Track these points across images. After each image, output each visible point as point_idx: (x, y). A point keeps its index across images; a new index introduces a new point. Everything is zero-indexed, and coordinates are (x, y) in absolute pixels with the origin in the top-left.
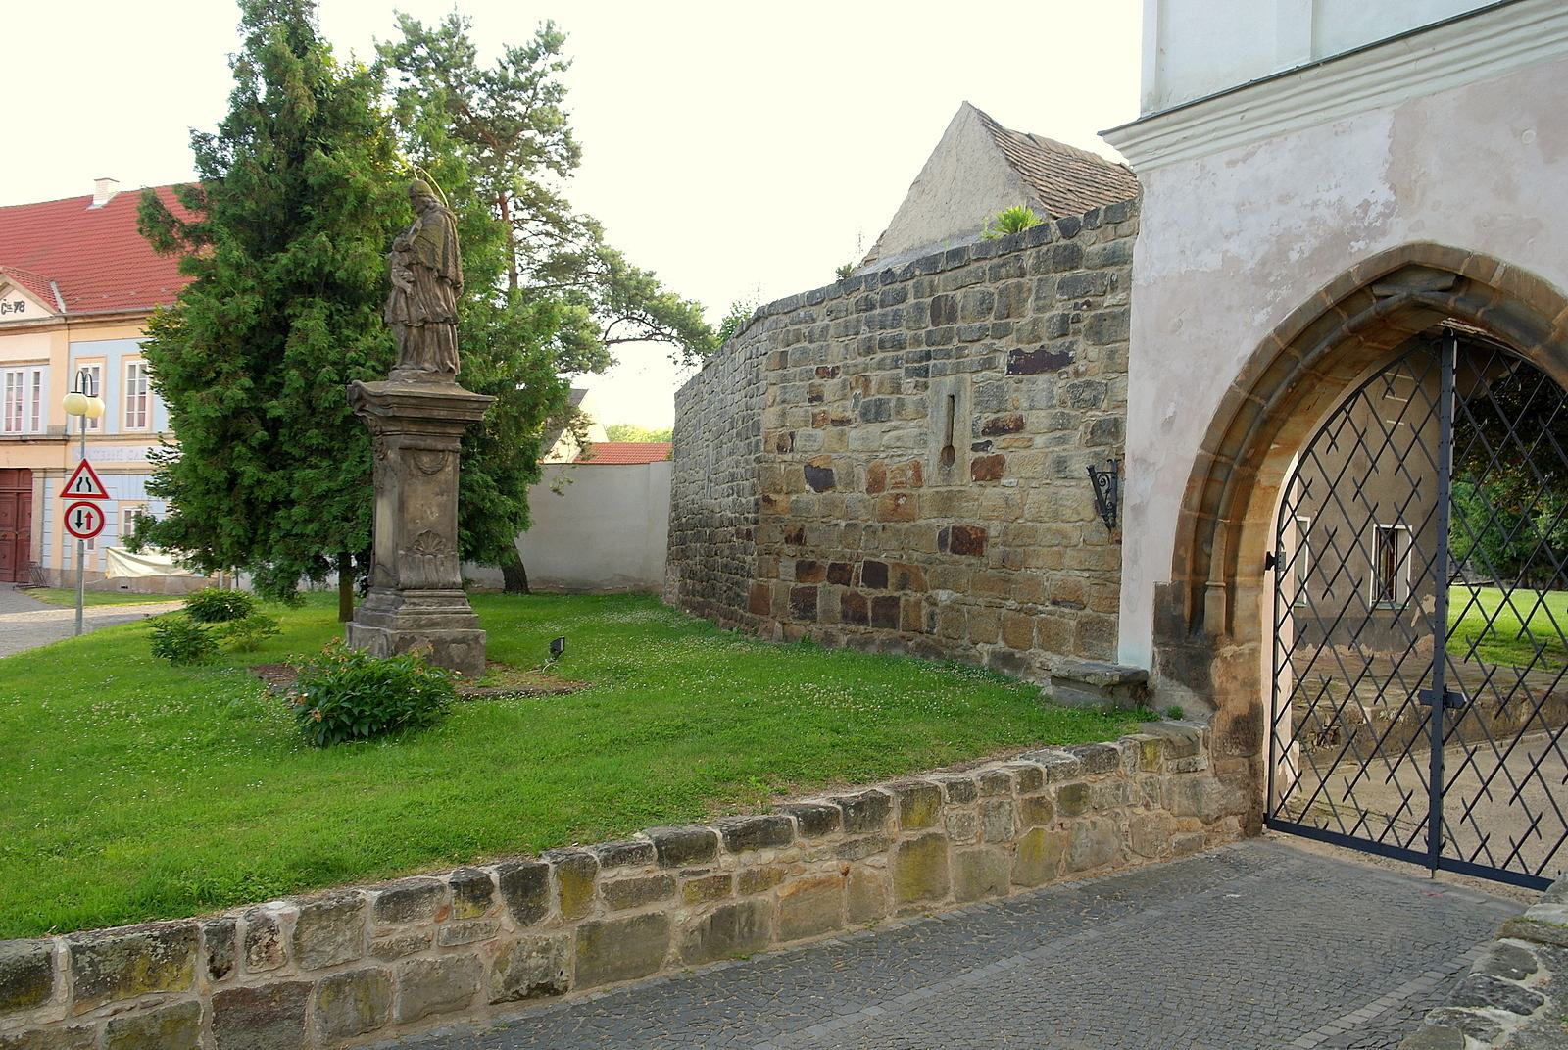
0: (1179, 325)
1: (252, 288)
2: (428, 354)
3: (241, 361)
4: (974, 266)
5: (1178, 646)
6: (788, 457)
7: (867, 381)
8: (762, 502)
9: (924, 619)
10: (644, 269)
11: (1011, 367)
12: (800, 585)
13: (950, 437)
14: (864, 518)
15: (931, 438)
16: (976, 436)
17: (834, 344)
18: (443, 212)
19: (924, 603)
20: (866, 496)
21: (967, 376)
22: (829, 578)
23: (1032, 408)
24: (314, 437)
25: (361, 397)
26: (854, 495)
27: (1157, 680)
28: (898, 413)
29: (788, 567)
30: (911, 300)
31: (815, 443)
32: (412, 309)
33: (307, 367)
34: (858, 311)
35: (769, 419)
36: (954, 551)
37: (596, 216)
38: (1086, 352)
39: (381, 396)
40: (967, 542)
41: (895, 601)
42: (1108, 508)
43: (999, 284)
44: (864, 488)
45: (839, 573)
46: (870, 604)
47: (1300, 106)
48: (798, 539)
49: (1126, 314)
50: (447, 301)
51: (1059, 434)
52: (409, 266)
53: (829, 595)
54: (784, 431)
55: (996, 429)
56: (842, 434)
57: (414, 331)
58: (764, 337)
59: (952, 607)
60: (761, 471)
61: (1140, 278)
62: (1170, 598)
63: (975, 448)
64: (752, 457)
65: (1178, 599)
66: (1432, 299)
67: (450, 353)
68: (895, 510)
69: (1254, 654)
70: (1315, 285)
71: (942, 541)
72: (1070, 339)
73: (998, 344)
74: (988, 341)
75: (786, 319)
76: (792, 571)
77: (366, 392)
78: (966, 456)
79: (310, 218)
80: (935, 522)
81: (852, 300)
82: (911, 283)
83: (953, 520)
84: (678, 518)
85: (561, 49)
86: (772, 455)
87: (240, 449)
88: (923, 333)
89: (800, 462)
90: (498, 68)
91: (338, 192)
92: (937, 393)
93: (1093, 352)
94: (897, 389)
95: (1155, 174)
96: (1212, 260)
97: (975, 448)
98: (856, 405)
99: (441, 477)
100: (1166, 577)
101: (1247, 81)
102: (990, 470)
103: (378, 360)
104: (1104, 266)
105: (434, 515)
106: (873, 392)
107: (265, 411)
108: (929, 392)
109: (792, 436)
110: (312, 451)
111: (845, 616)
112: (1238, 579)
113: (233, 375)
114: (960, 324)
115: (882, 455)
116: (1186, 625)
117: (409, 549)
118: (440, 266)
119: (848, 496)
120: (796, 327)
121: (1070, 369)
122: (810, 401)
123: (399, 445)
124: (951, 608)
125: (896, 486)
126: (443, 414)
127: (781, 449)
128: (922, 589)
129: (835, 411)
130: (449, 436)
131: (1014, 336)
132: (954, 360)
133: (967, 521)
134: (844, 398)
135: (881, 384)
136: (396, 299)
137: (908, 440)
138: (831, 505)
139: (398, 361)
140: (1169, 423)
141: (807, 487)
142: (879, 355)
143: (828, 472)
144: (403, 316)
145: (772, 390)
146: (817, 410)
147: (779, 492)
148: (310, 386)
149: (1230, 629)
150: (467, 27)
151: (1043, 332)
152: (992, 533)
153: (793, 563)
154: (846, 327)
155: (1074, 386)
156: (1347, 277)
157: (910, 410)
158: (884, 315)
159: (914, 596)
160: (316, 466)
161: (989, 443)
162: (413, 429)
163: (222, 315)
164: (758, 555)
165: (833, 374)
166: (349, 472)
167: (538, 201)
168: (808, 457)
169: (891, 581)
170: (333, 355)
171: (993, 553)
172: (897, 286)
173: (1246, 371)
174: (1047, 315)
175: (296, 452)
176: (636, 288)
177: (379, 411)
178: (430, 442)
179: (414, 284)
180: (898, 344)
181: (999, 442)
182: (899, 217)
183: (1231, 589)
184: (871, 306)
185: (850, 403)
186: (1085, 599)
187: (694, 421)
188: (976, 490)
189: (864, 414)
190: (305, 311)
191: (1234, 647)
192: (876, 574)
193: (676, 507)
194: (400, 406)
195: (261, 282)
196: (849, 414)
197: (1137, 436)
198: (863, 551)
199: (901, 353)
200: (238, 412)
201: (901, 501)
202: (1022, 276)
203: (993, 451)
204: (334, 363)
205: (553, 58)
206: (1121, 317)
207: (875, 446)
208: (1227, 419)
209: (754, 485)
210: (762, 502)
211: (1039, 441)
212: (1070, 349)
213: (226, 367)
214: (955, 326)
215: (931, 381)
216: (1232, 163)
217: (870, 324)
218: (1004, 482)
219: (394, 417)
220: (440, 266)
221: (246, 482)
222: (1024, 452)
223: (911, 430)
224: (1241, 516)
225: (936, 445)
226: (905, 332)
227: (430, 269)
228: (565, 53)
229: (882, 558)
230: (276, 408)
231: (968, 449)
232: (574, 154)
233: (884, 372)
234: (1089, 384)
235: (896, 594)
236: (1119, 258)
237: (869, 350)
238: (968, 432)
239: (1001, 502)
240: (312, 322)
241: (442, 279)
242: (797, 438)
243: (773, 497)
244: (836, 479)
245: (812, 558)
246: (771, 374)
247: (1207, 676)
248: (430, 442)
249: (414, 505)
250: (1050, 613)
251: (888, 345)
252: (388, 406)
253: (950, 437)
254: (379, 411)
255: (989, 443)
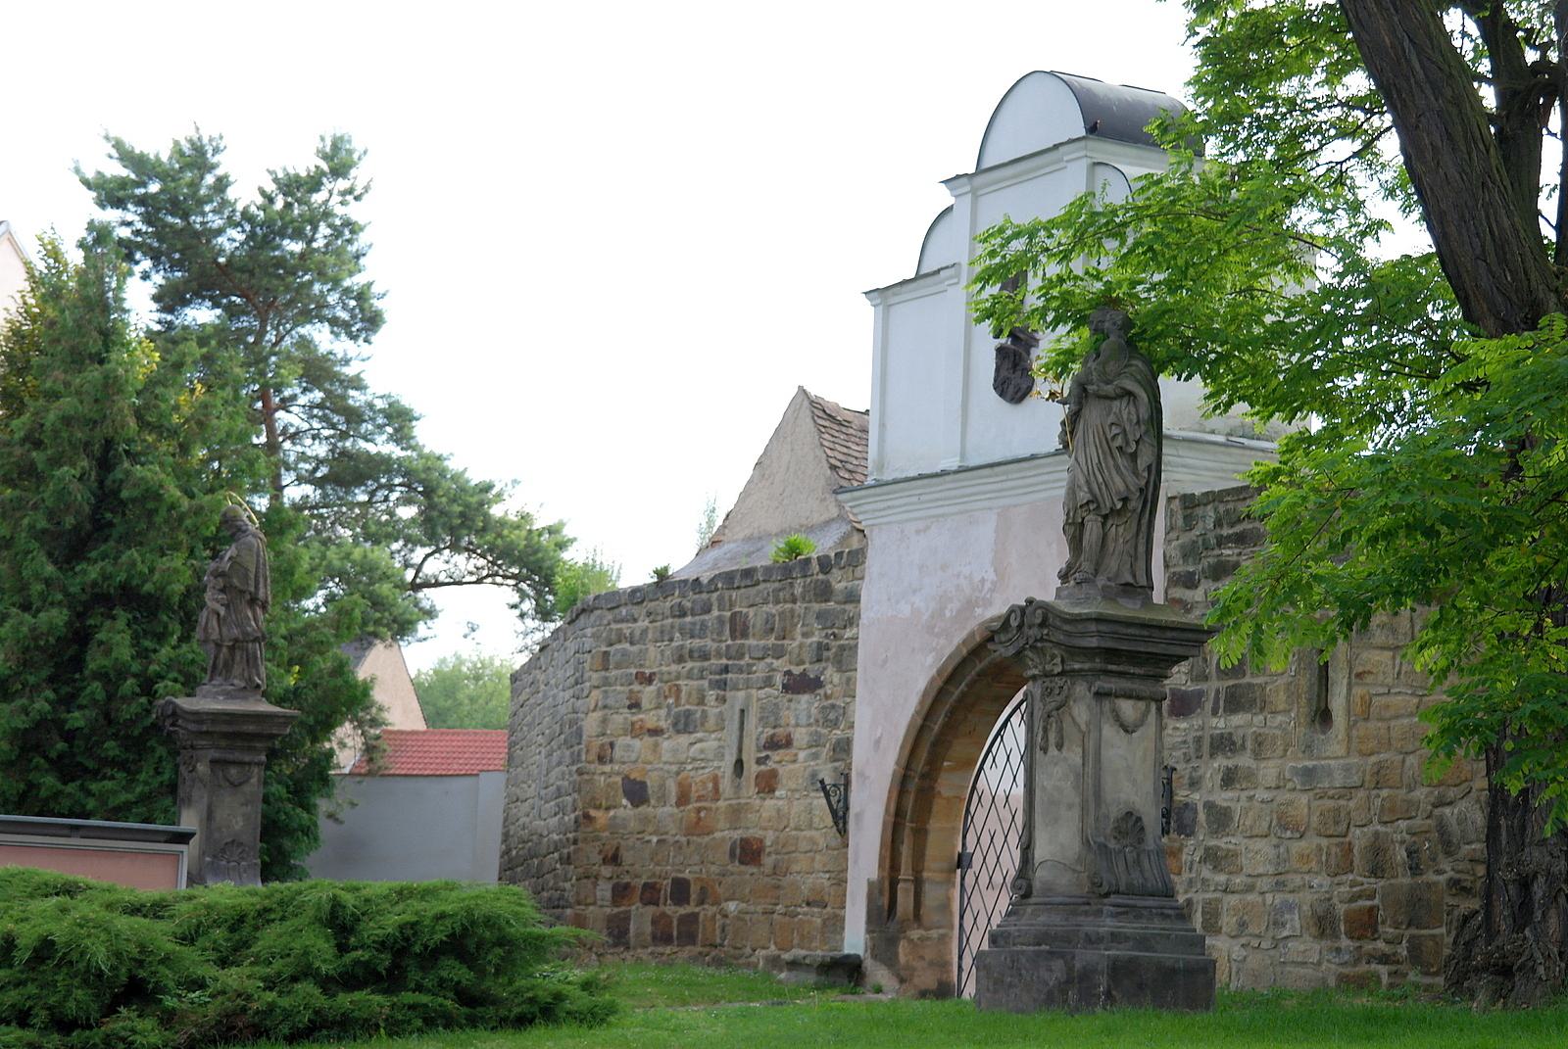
0: (885, 661)
1: (60, 603)
2: (237, 670)
3: (45, 673)
4: (762, 586)
6: (607, 768)
7: (679, 690)
8: (581, 820)
9: (718, 932)
10: (475, 478)
11: (785, 686)
12: (616, 910)
13: (740, 750)
14: (674, 834)
15: (727, 752)
16: (759, 751)
17: (652, 648)
18: (255, 536)
19: (718, 917)
20: (676, 810)
21: (754, 691)
22: (641, 899)
23: (797, 725)
24: (111, 748)
25: (176, 714)
26: (665, 809)
27: (869, 964)
28: (702, 724)
29: (604, 890)
30: (715, 613)
31: (632, 750)
32: (224, 630)
33: (111, 679)
34: (674, 617)
35: (591, 724)
36: (742, 862)
37: (406, 402)
38: (831, 675)
39: (196, 713)
40: (749, 852)
41: (695, 916)
42: (840, 818)
43: (778, 607)
44: (673, 800)
45: (650, 894)
46: (675, 923)
47: (955, 497)
48: (614, 859)
49: (856, 646)
50: (255, 620)
51: (814, 750)
52: (223, 591)
53: (641, 919)
54: (606, 740)
55: (773, 744)
56: (656, 745)
57: (225, 650)
58: (589, 631)
59: (740, 917)
60: (582, 782)
61: (864, 621)
63: (759, 761)
64: (574, 768)
65: (881, 892)
67: (257, 670)
68: (697, 823)
69: (944, 939)
70: (959, 637)
71: (732, 854)
72: (824, 664)
73: (776, 663)
74: (769, 660)
75: (610, 616)
76: (608, 894)
77: (182, 709)
78: (752, 769)
79: (111, 524)
80: (726, 834)
81: (668, 604)
82: (715, 595)
83: (739, 832)
84: (507, 852)
85: (353, 172)
86: (592, 766)
87: (38, 760)
88: (723, 645)
89: (618, 774)
90: (260, 200)
91: (150, 505)
92: (732, 707)
93: (836, 678)
94: (701, 701)
95: (876, 530)
96: (905, 610)
97: (759, 761)
98: (668, 714)
99: (246, 788)
100: (874, 875)
102: (768, 784)
103: (180, 672)
104: (845, 603)
105: (238, 824)
106: (683, 701)
107: (65, 721)
108: (726, 706)
109: (612, 745)
110: (113, 763)
111: (654, 938)
112: (925, 874)
113: (36, 689)
114: (751, 642)
115: (689, 767)
116: (885, 914)
117: (215, 856)
118: (252, 589)
119: (660, 810)
120: (619, 626)
121: (821, 691)
122: (630, 707)
123: (209, 757)
124: (738, 918)
125: (700, 799)
126: (251, 728)
127: (601, 759)
128: (716, 903)
129: (651, 719)
130: (255, 749)
131: (786, 658)
132: (744, 676)
133: (753, 833)
134: (658, 707)
135: (690, 694)
136: (207, 619)
137: (705, 753)
138: (645, 820)
139: (208, 677)
140: (878, 742)
141: (624, 802)
142: (689, 665)
143: (643, 785)
144: (215, 636)
145: (595, 693)
146: (635, 718)
147: (598, 807)
148: (110, 697)
149: (917, 915)
150: (216, 151)
151: (806, 656)
152: (768, 843)
153: (609, 886)
154: (662, 632)
155: (824, 708)
156: (972, 635)
157: (711, 722)
158: (694, 624)
159: (710, 910)
160: (112, 778)
161: (767, 757)
162: (223, 743)
163: (33, 629)
164: (578, 880)
165: (649, 680)
166: (146, 783)
167: (317, 370)
168: (626, 768)
169: (693, 896)
170: (136, 667)
171: (768, 861)
172: (704, 596)
173: (921, 702)
174: (809, 641)
175: (91, 764)
176: (462, 515)
177: (192, 727)
178: (237, 756)
179: (227, 606)
180: (705, 656)
181: (776, 756)
182: (744, 496)
183: (918, 883)
184: (683, 615)
185: (663, 712)
186: (826, 898)
187: (529, 718)
188: (758, 802)
189: (675, 724)
190: (108, 623)
191: (921, 932)
192: (681, 891)
193: (506, 836)
194: (213, 721)
195: (67, 594)
196: (663, 724)
197: (859, 754)
198: (668, 870)
199: (706, 664)
200: (41, 724)
201: (702, 814)
202: (794, 601)
203: (771, 765)
204: (135, 676)
205: (342, 184)
206: (853, 649)
207: (683, 757)
208: (911, 741)
209: (575, 800)
210: (581, 820)
211: (802, 755)
212: (822, 673)
213: (32, 679)
214: (747, 642)
215: (729, 694)
216: (918, 532)
217: (682, 631)
218: (777, 793)
219: (207, 732)
220: (252, 589)
221: (43, 793)
222: (792, 766)
223: (711, 744)
224: (926, 821)
225: (730, 759)
226: (709, 643)
227: (242, 592)
228: (359, 176)
229: (686, 875)
230: (77, 719)
231: (753, 762)
232: (373, 321)
233: (691, 683)
234: (833, 706)
235: (697, 910)
236: (853, 598)
237: (681, 660)
238: (754, 748)
239: (774, 814)
240: (116, 638)
241: (253, 601)
242: (617, 748)
243: (593, 813)
244: (650, 792)
245: (626, 879)
246: (595, 676)
247: (896, 954)
248: (237, 756)
249: (220, 815)
250: (805, 914)
251: (696, 655)
252: (201, 722)
253: (740, 750)
254: (192, 727)
255: (767, 757)
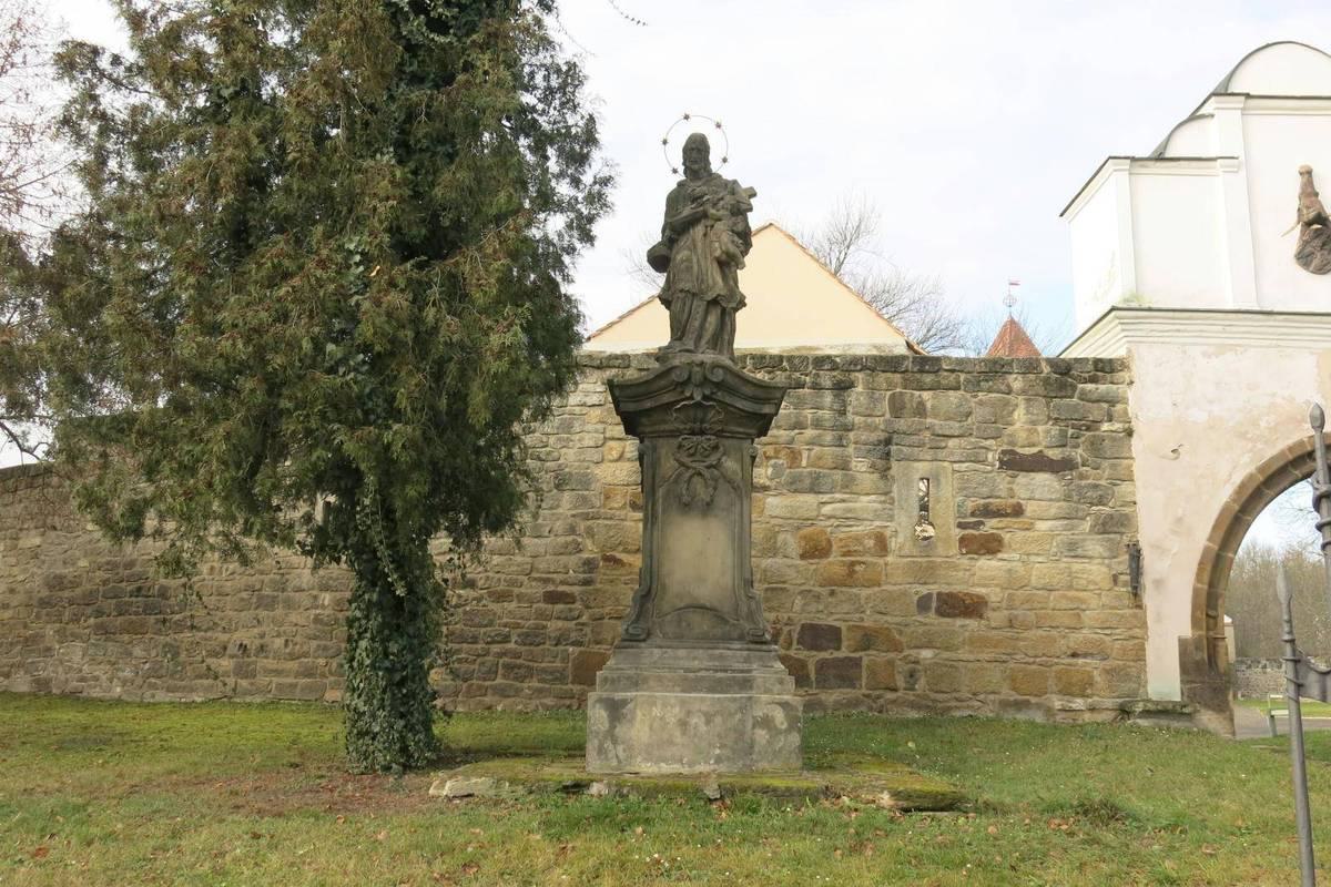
5: (1203, 682)
41: (857, 663)
62: (1192, 648)
66: (714, 279)
101: (1244, 308)
171: (996, 618)
